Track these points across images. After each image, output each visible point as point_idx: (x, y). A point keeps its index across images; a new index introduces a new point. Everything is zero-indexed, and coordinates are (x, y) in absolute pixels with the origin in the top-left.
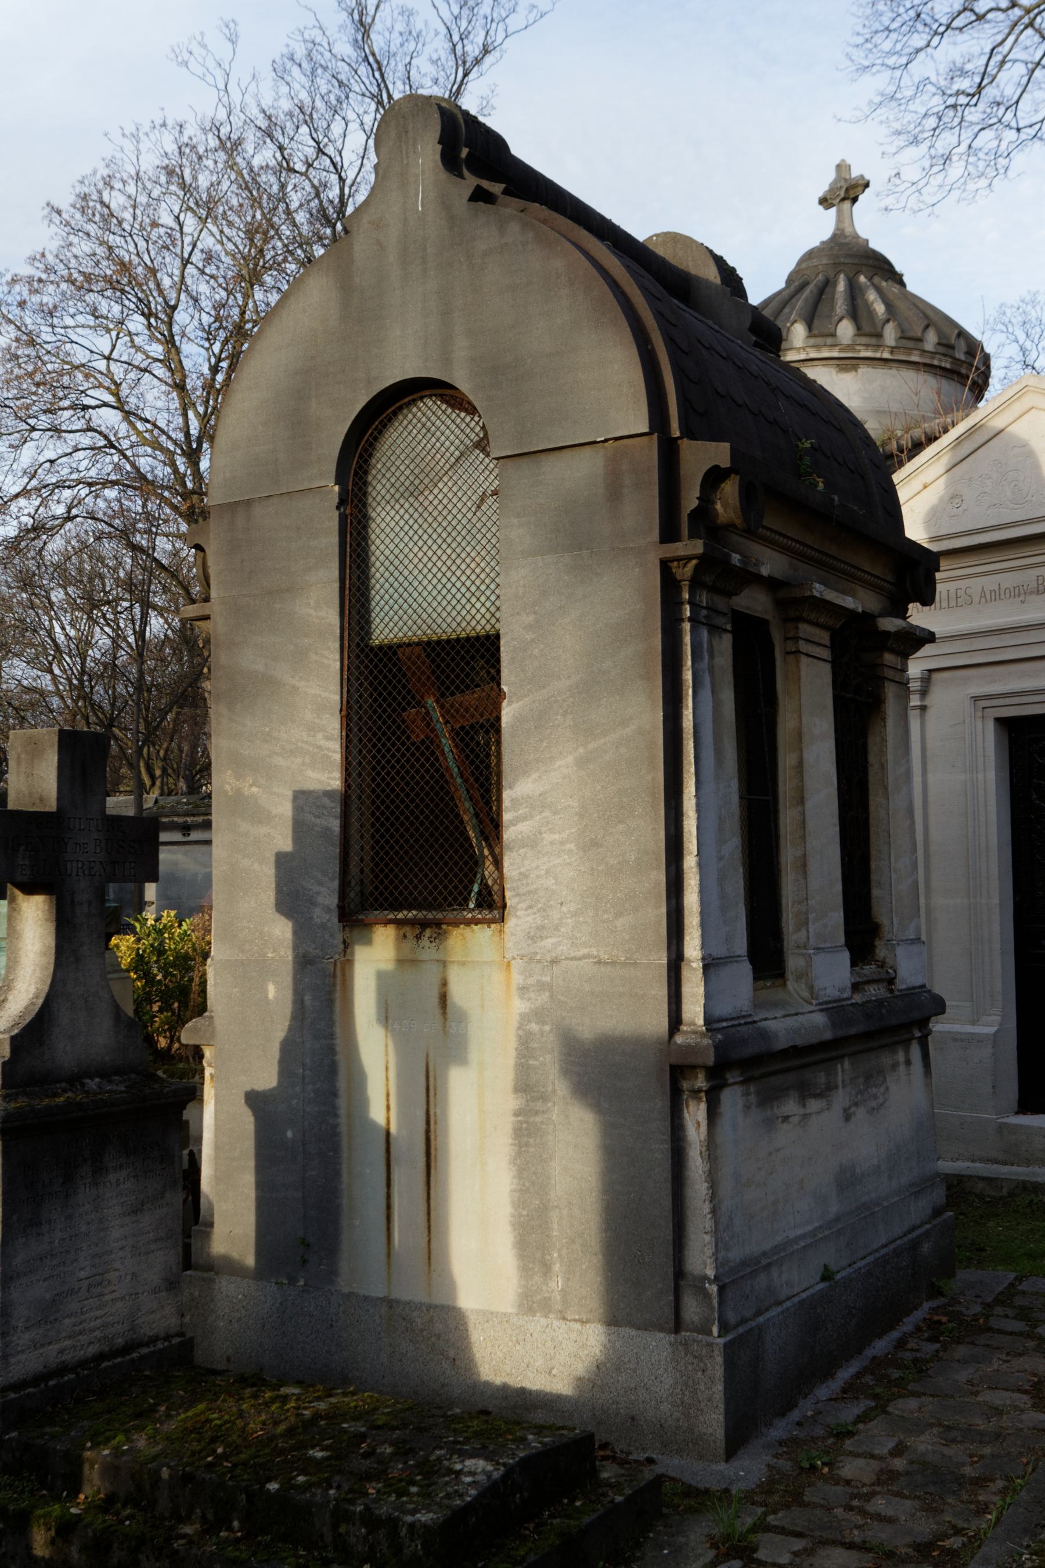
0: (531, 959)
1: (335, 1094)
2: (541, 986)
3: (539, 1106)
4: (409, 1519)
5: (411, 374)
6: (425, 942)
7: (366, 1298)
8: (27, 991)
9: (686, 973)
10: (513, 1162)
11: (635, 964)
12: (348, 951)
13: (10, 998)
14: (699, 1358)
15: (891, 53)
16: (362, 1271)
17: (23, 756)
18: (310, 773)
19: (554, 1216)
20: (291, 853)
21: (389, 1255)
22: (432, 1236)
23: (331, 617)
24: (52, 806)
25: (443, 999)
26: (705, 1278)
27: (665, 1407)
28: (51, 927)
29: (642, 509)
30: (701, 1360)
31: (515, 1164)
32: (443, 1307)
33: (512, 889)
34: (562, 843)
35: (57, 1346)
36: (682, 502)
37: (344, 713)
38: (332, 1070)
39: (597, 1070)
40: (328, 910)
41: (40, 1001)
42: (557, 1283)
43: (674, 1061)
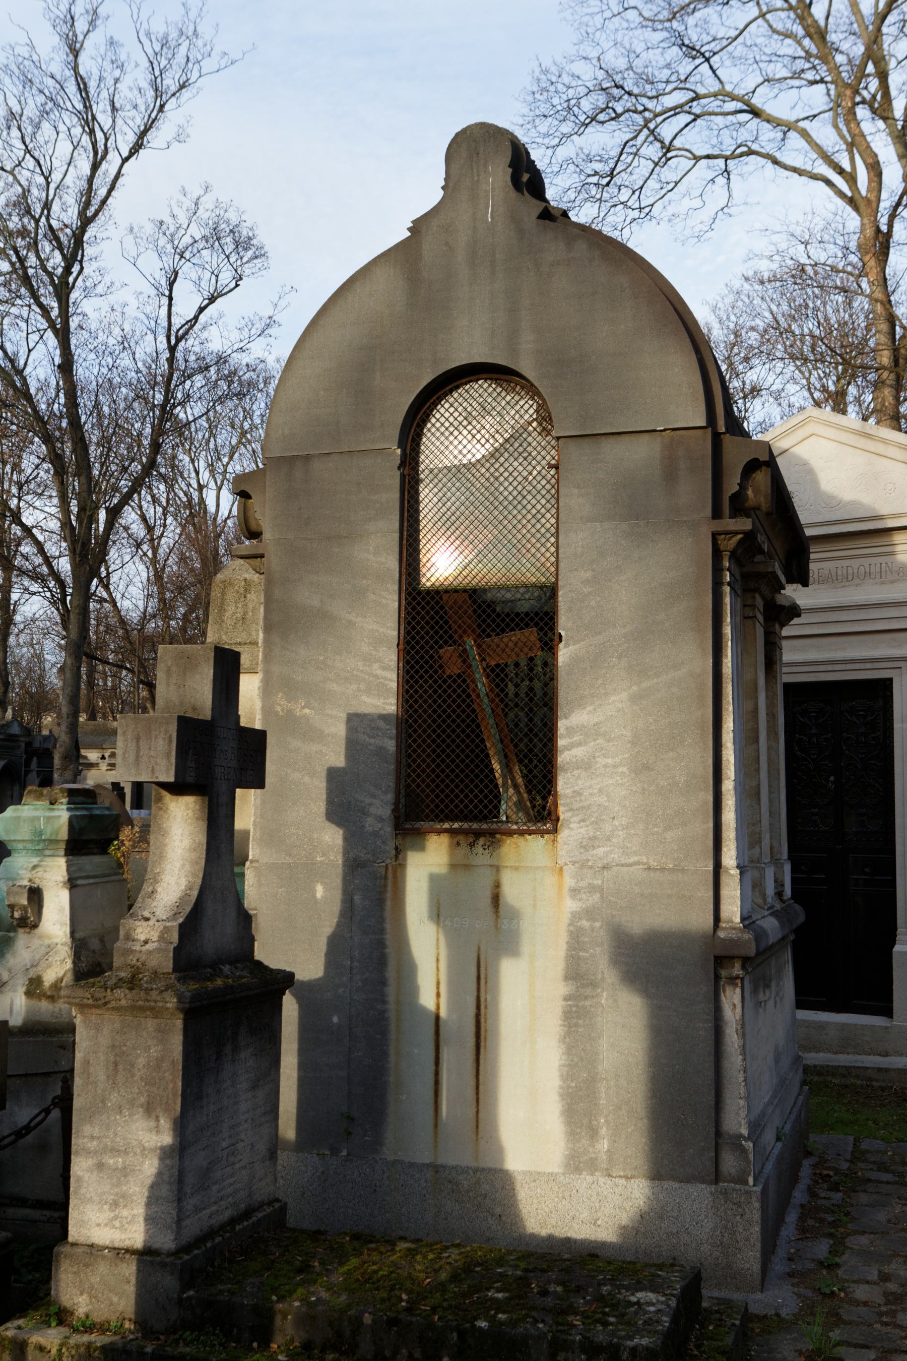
0: (583, 865)
1: (383, 982)
2: (592, 889)
3: (588, 991)
4: (630, 1343)
5: (477, 359)
6: (479, 849)
7: (412, 1165)
8: (177, 883)
9: (724, 879)
10: (563, 1040)
11: (683, 870)
12: (400, 856)
13: (159, 889)
14: (738, 1204)
15: (547, 135)
16: (409, 1140)
17: (174, 669)
18: (365, 698)
19: (602, 1087)
20: (343, 768)
21: (436, 1126)
22: (480, 1107)
23: (391, 563)
24: (209, 718)
25: (496, 899)
26: (741, 1136)
27: (706, 1248)
28: (203, 825)
29: (695, 491)
30: (740, 1206)
31: (564, 1043)
32: (490, 1170)
33: (564, 805)
34: (615, 766)
35: (208, 1211)
36: (724, 485)
37: (401, 647)
38: (382, 962)
39: (647, 961)
40: (380, 819)
41: (195, 893)
42: (604, 1145)
43: (718, 952)
